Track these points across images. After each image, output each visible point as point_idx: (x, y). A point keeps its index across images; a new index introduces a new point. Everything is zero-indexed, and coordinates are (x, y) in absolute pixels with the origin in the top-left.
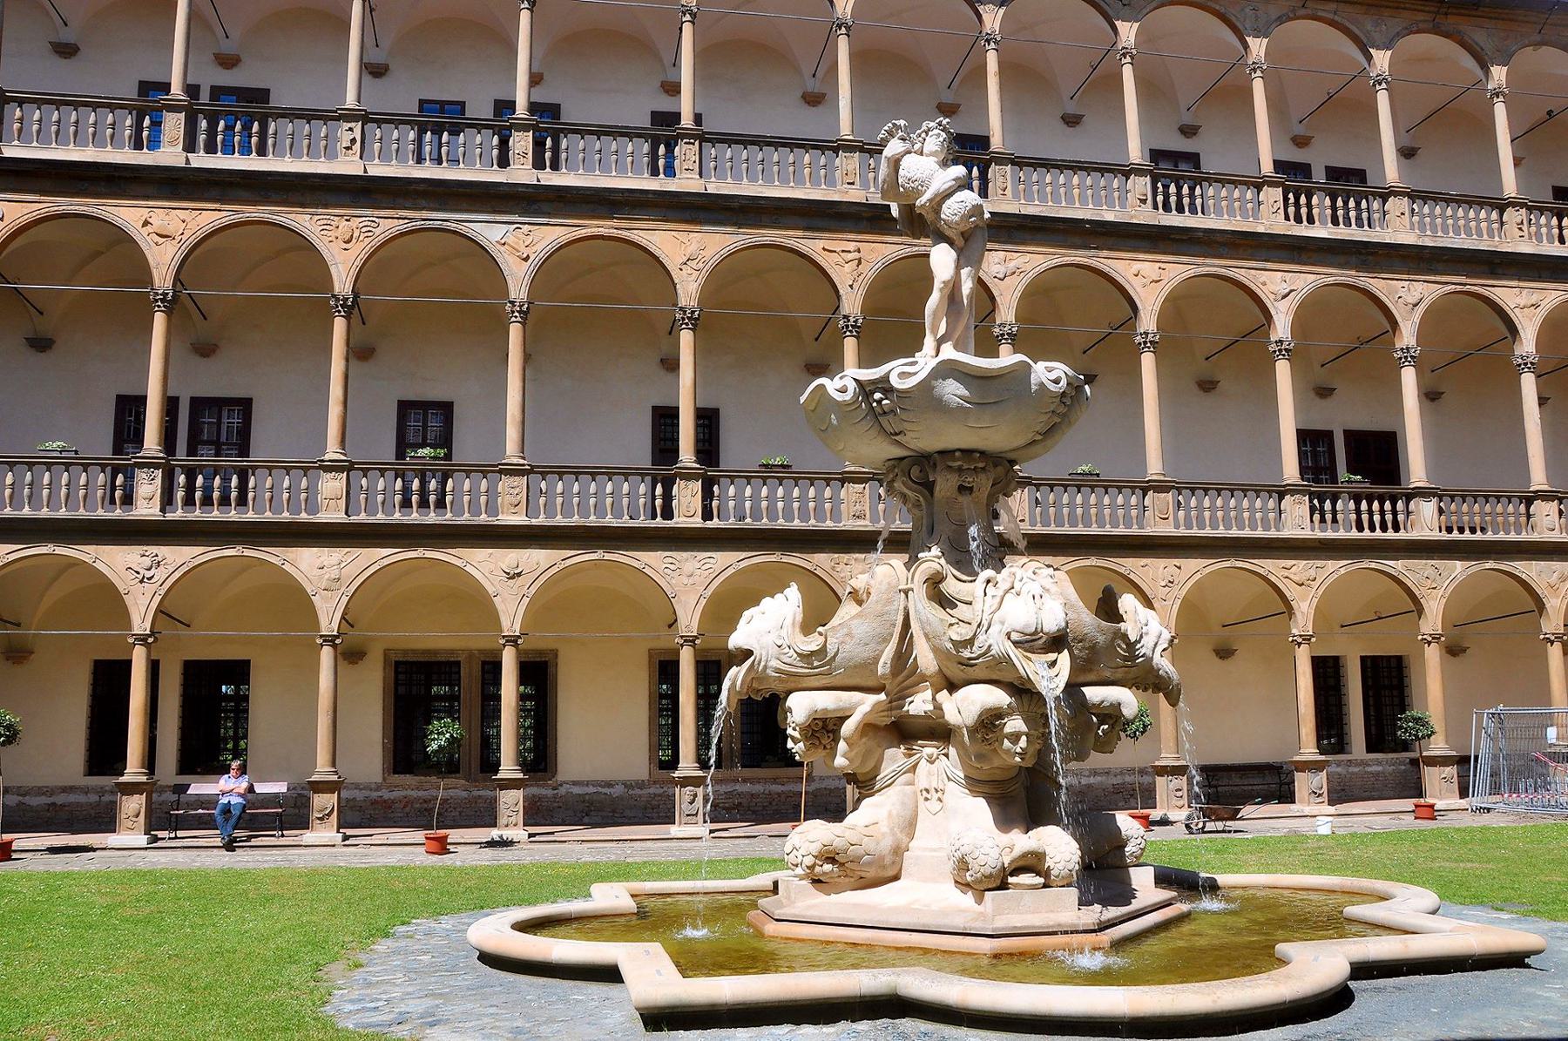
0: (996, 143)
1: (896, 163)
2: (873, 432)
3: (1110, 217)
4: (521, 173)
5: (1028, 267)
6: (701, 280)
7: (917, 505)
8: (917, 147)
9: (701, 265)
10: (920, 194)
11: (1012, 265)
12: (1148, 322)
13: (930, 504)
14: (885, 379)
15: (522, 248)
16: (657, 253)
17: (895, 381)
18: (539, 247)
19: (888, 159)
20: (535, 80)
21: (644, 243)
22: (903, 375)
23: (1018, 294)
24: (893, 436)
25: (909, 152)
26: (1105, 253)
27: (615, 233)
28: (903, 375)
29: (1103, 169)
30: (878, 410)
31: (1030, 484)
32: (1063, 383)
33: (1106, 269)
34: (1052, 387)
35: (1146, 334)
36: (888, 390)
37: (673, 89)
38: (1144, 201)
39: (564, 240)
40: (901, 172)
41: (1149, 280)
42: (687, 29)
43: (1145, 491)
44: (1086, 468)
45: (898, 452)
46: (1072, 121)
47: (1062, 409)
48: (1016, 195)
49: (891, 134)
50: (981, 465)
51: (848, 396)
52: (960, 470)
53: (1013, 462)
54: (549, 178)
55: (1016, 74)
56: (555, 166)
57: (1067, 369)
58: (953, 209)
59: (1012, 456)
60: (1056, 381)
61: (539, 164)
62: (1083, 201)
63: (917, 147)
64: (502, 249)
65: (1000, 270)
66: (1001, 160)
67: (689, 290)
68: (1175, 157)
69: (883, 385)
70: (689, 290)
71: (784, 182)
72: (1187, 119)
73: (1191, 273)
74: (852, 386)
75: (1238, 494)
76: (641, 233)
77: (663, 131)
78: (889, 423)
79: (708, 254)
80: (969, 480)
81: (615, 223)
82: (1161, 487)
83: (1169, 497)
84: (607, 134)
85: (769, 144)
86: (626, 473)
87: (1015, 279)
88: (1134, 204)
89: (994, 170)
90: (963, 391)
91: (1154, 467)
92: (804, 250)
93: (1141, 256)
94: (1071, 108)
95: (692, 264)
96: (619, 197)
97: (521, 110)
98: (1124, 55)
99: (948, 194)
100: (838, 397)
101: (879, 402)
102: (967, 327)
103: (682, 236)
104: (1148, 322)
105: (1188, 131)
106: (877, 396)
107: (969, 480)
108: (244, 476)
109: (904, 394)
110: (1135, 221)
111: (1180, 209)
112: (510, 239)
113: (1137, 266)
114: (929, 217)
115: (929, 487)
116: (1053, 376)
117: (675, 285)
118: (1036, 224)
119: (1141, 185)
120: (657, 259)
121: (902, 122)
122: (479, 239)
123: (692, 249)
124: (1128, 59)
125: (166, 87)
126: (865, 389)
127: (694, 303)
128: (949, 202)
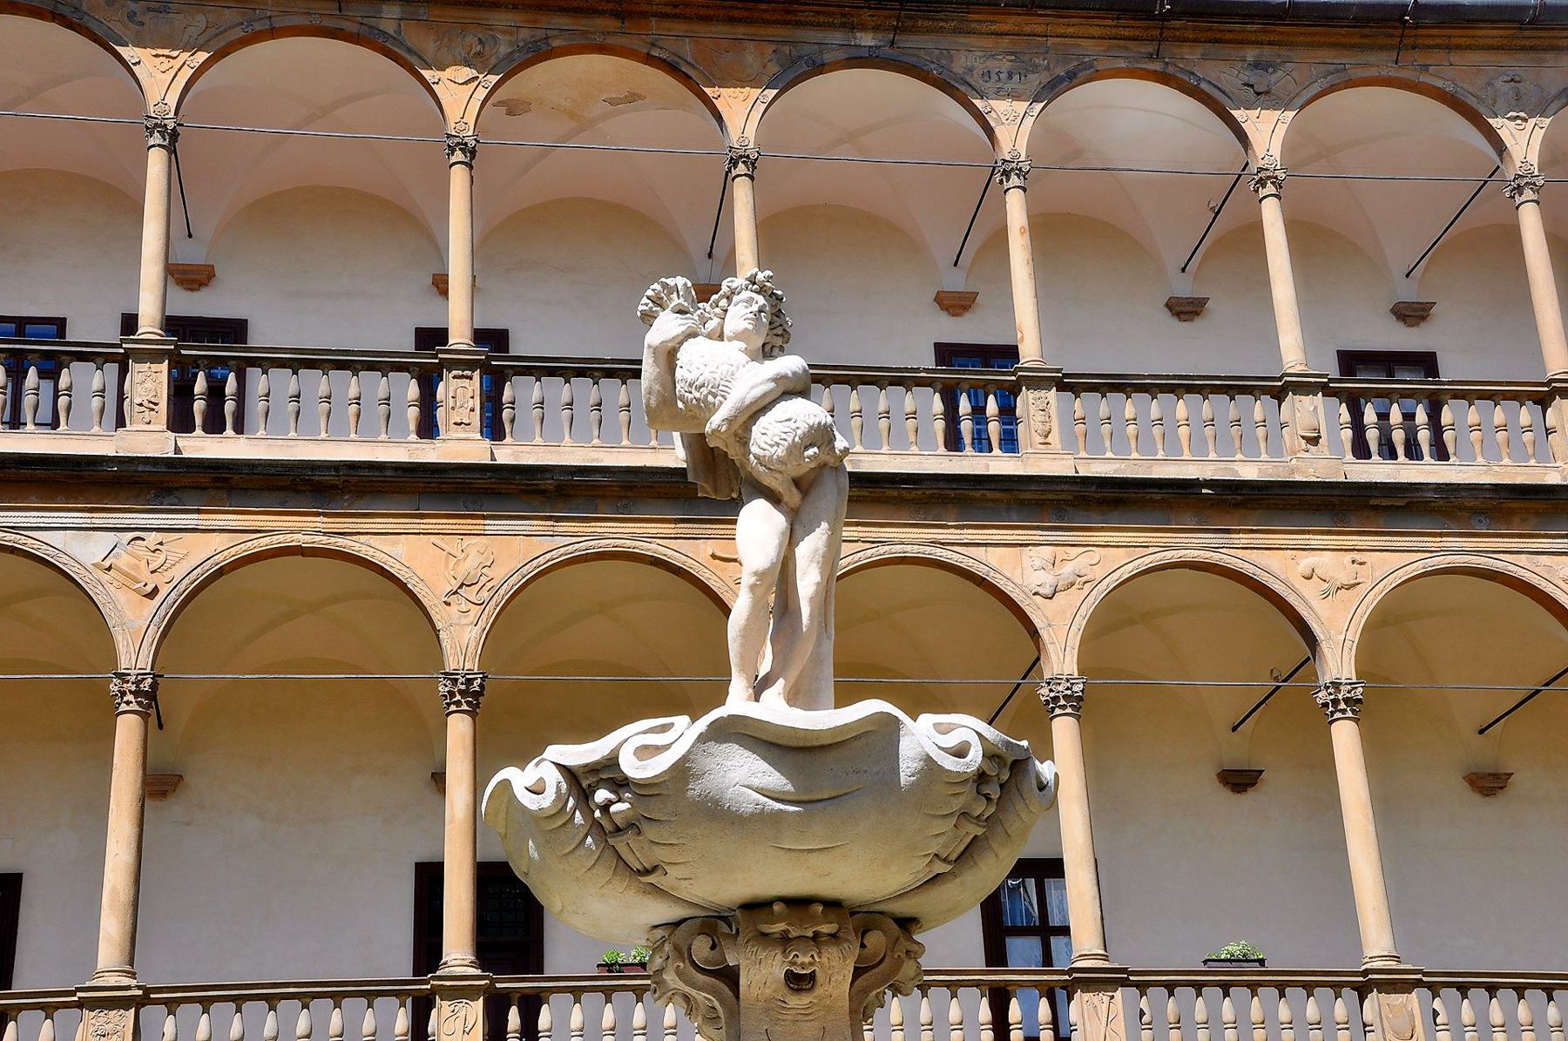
0: (1029, 353)
1: (669, 356)
2: (604, 872)
3: (1249, 472)
4: (461, 445)
5: (1098, 573)
6: (486, 621)
7: (712, 1019)
8: (711, 325)
9: (485, 595)
10: (712, 409)
11: (1067, 570)
12: (1338, 663)
13: (734, 1013)
14: (611, 762)
15: (145, 575)
16: (402, 575)
17: (631, 767)
18: (178, 572)
19: (655, 350)
20: (184, 276)
21: (378, 558)
22: (645, 752)
23: (1081, 622)
24: (643, 875)
25: (693, 335)
26: (1244, 539)
27: (321, 541)
28: (645, 752)
29: (1233, 388)
30: (608, 826)
31: (1125, 983)
32: (975, 756)
33: (1249, 570)
34: (949, 763)
35: (1336, 685)
36: (620, 784)
37: (441, 285)
38: (1314, 441)
39: (223, 559)
40: (679, 373)
41: (1336, 585)
42: (459, 178)
43: (1362, 991)
44: (1235, 949)
45: (674, 913)
46: (1186, 309)
47: (979, 808)
48: (1069, 443)
49: (658, 302)
50: (826, 929)
51: (547, 800)
52: (785, 941)
53: (907, 924)
54: (201, 446)
55: (1047, 230)
56: (214, 425)
57: (983, 727)
58: (775, 433)
59: (904, 908)
60: (960, 752)
61: (180, 421)
62: (1198, 445)
63: (711, 325)
64: (105, 577)
65: (1045, 580)
66: (1039, 382)
67: (462, 640)
68: (1388, 362)
69: (608, 772)
70: (462, 640)
71: (583, 440)
72: (1409, 292)
73: (1418, 568)
74: (553, 778)
75: (1479, 994)
76: (372, 540)
77: (977, 375)
78: (635, 850)
79: (498, 573)
80: (803, 960)
81: (319, 522)
82: (1396, 984)
83: (1413, 1001)
84: (311, 365)
85: (610, 374)
86: (370, 993)
87: (1075, 596)
88: (1308, 443)
89: (1027, 401)
90: (774, 779)
91: (1377, 943)
92: (678, 560)
93: (1316, 540)
94: (1184, 288)
95: (470, 593)
96: (329, 478)
97: (459, 338)
98: (1262, 183)
99: (760, 408)
100: (530, 802)
101: (605, 808)
102: (816, 660)
103: (452, 544)
104: (1338, 663)
105: (1411, 314)
106: (602, 795)
107: (803, 960)
108: (531, 1005)
109: (645, 791)
110: (1298, 478)
111: (1389, 452)
112: (123, 560)
113: (1307, 561)
114: (733, 452)
115: (730, 977)
116: (951, 740)
117: (436, 632)
118: (1109, 493)
119: (1306, 410)
120: (403, 586)
121: (680, 281)
122: (62, 562)
123: (469, 565)
124: (1270, 189)
125: (1011, 353)
126: (579, 781)
127: (472, 665)
128: (763, 421)
